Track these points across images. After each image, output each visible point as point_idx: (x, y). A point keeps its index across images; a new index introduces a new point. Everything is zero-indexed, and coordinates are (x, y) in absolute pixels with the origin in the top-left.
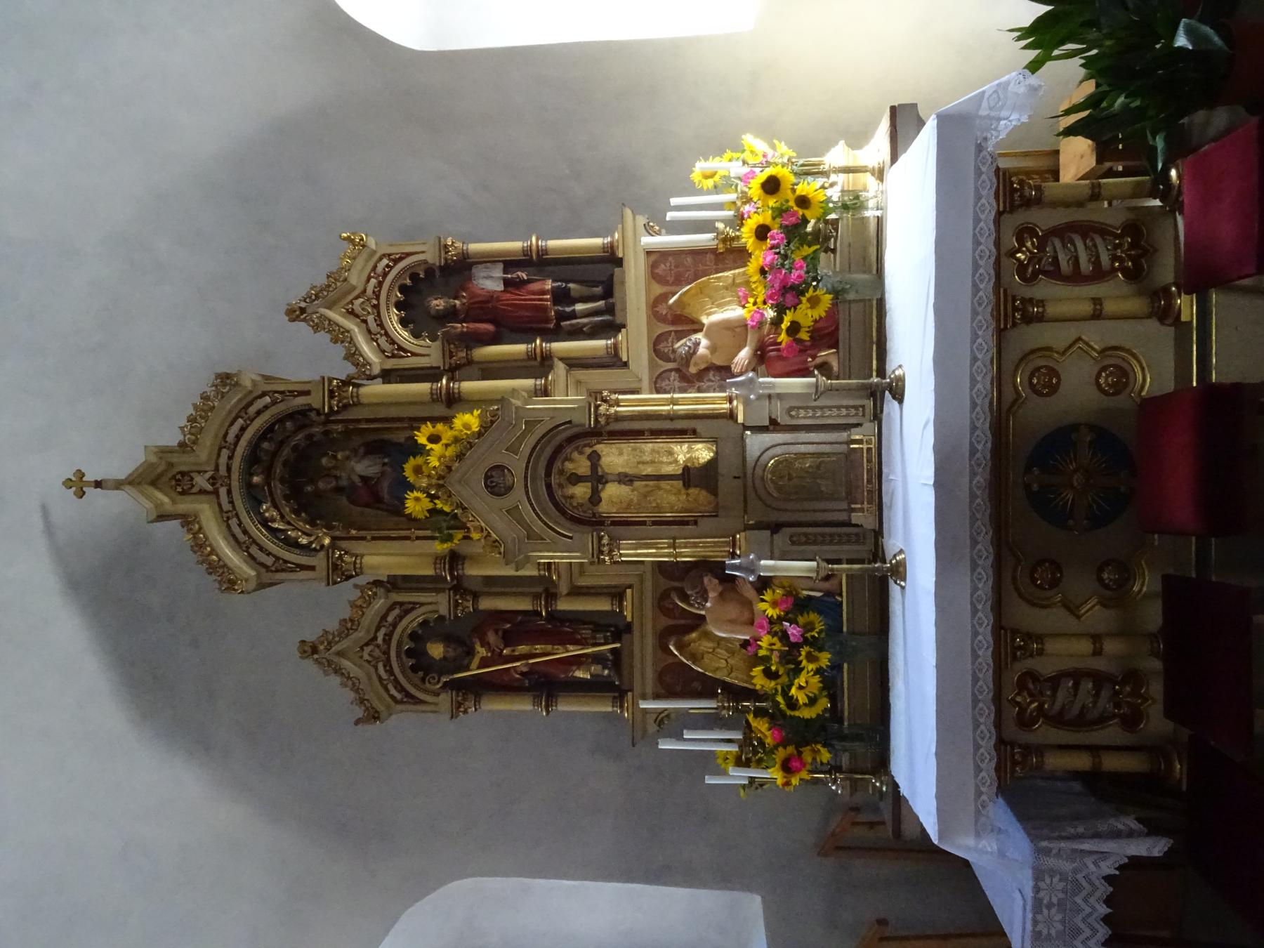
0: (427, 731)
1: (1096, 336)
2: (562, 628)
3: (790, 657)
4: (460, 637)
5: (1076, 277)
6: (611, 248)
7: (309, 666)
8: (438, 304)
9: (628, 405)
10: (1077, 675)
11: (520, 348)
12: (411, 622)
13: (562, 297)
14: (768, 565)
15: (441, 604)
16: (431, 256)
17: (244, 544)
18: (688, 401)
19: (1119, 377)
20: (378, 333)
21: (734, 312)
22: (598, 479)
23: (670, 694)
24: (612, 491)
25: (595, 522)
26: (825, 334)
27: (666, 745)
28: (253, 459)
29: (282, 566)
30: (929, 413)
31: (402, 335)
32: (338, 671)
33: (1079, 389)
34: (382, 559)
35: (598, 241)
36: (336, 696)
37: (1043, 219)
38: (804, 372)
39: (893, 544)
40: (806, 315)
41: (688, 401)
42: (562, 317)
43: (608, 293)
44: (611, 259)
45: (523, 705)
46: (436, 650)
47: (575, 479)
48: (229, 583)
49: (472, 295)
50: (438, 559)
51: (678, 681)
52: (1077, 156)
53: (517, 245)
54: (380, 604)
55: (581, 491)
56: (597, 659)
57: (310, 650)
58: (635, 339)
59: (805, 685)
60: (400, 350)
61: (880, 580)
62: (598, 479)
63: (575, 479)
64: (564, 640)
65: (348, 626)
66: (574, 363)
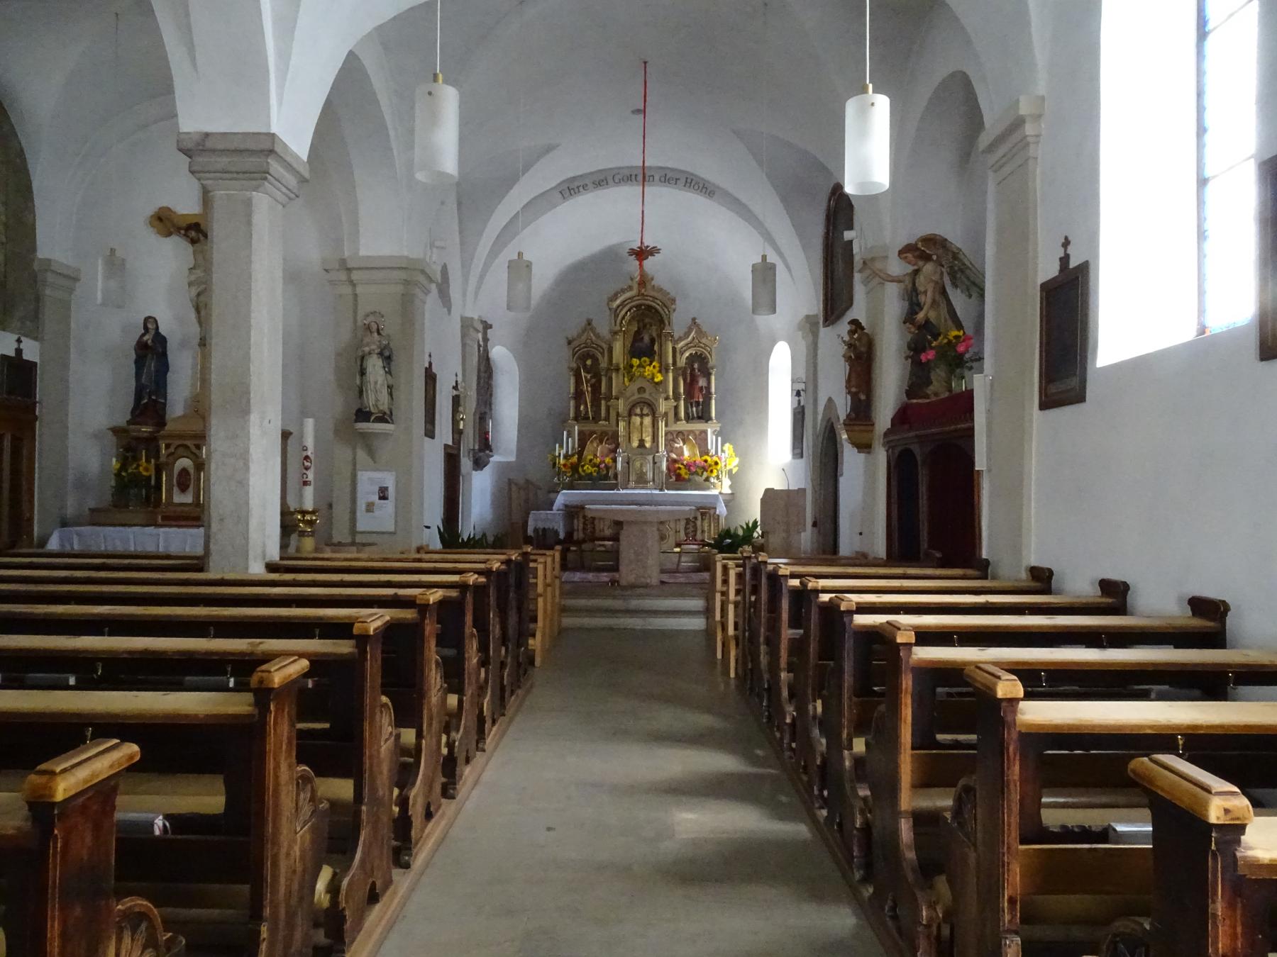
0: (563, 359)
5: (686, 529)
6: (710, 419)
8: (696, 366)
9: (662, 425)
13: (698, 403)
15: (604, 364)
16: (711, 363)
17: (623, 304)
18: (662, 441)
20: (688, 346)
21: (686, 453)
22: (642, 416)
24: (638, 419)
25: (630, 415)
26: (679, 477)
28: (649, 308)
31: (687, 354)
34: (618, 348)
36: (573, 333)
38: (668, 468)
40: (683, 472)
41: (662, 441)
46: (589, 362)
52: (948, 815)
54: (605, 346)
55: (638, 411)
57: (589, 323)
59: (588, 468)
62: (642, 416)
64: (592, 402)
65: (598, 336)
66: (676, 408)
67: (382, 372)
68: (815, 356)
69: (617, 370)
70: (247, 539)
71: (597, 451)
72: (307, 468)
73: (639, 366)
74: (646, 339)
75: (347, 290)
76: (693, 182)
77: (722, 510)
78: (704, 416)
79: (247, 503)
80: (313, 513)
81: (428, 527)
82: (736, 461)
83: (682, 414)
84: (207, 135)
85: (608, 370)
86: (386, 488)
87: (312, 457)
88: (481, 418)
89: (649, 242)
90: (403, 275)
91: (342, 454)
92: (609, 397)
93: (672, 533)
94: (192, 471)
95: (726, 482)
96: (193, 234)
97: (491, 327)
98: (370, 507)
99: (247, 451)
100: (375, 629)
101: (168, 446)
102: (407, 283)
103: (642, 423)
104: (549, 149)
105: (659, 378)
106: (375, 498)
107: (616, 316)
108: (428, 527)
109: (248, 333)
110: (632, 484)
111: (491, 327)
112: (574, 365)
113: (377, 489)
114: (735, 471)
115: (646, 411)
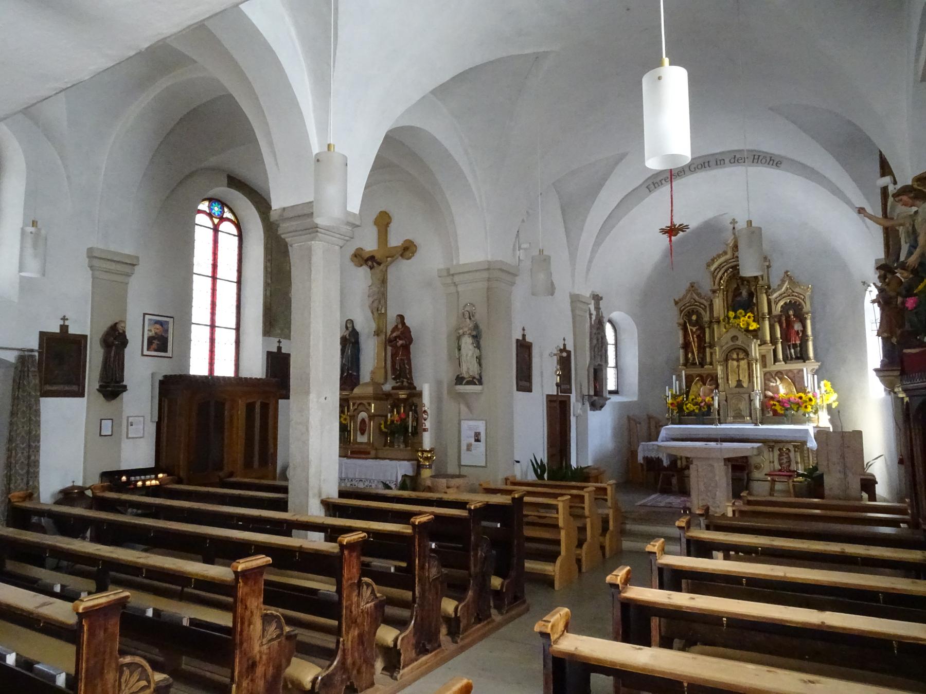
0: (673, 317)
2: (702, 349)
3: (696, 404)
4: (699, 324)
5: (780, 460)
6: (808, 359)
7: (688, 285)
8: (791, 312)
11: (779, 335)
12: (702, 312)
13: (795, 346)
14: (716, 398)
15: (706, 318)
16: (805, 310)
17: (719, 267)
19: (758, 467)
20: (781, 297)
22: (738, 360)
23: (686, 378)
24: (735, 363)
26: (775, 413)
27: (674, 377)
29: (714, 278)
31: (782, 303)
32: (687, 293)
34: (718, 303)
40: (778, 408)
42: (789, 346)
43: (797, 358)
45: (681, 341)
46: (694, 317)
47: (738, 355)
48: (709, 265)
49: (794, 322)
50: (719, 318)
51: (689, 380)
54: (706, 304)
55: (735, 356)
56: (694, 359)
58: (781, 366)
59: (691, 407)
62: (738, 360)
65: (699, 295)
66: (775, 351)
67: (471, 347)
69: (718, 322)
70: (307, 482)
71: (700, 391)
73: (735, 317)
74: (744, 293)
75: (452, 289)
78: (802, 357)
79: (308, 457)
80: (430, 451)
81: (518, 462)
82: (834, 396)
83: (780, 356)
84: (284, 209)
85: (711, 322)
86: (479, 433)
87: (429, 412)
88: (596, 371)
89: (677, 222)
90: (485, 275)
91: (450, 407)
92: (712, 346)
93: (767, 463)
94: (367, 420)
96: (370, 263)
97: (601, 298)
98: (469, 447)
99: (308, 421)
100: (84, 609)
101: (354, 404)
102: (489, 280)
103: (738, 366)
104: (622, 157)
105: (754, 326)
106: (472, 440)
107: (714, 278)
108: (518, 462)
109: (309, 338)
110: (730, 419)
112: (681, 321)
113: (473, 435)
114: (834, 405)
115: (741, 356)
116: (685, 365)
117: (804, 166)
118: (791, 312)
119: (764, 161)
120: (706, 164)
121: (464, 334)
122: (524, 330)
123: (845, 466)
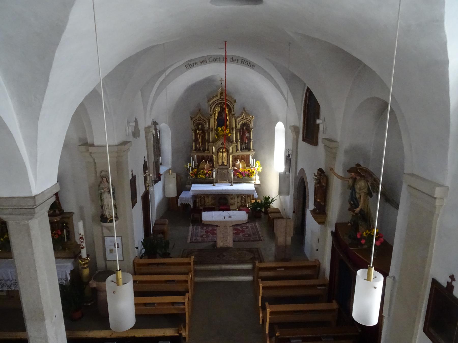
0: (190, 125)
1: (236, 203)
2: (203, 143)
5: (241, 201)
6: (249, 149)
8: (245, 128)
10: (205, 201)
11: (239, 138)
13: (246, 143)
15: (206, 127)
16: (251, 127)
17: (213, 103)
21: (241, 166)
22: (223, 152)
24: (221, 154)
30: (229, 189)
31: (241, 123)
33: (231, 201)
35: (252, 148)
37: (246, 198)
39: (216, 184)
40: (240, 176)
44: (249, 149)
46: (200, 127)
47: (223, 150)
48: (209, 101)
53: (252, 138)
54: (206, 120)
55: (221, 150)
56: (200, 147)
58: (240, 153)
60: (239, 123)
61: (212, 182)
62: (223, 152)
63: (223, 150)
66: (237, 146)
68: (297, 148)
72: (82, 242)
76: (244, 62)
77: (256, 196)
78: (248, 149)
95: (257, 177)
103: (223, 155)
107: (211, 108)
111: (158, 124)
112: (194, 128)
116: (195, 150)
117: (265, 72)
118: (245, 128)
119: (246, 64)
120: (218, 59)
121: (104, 192)
122: (132, 171)
123: (286, 233)
